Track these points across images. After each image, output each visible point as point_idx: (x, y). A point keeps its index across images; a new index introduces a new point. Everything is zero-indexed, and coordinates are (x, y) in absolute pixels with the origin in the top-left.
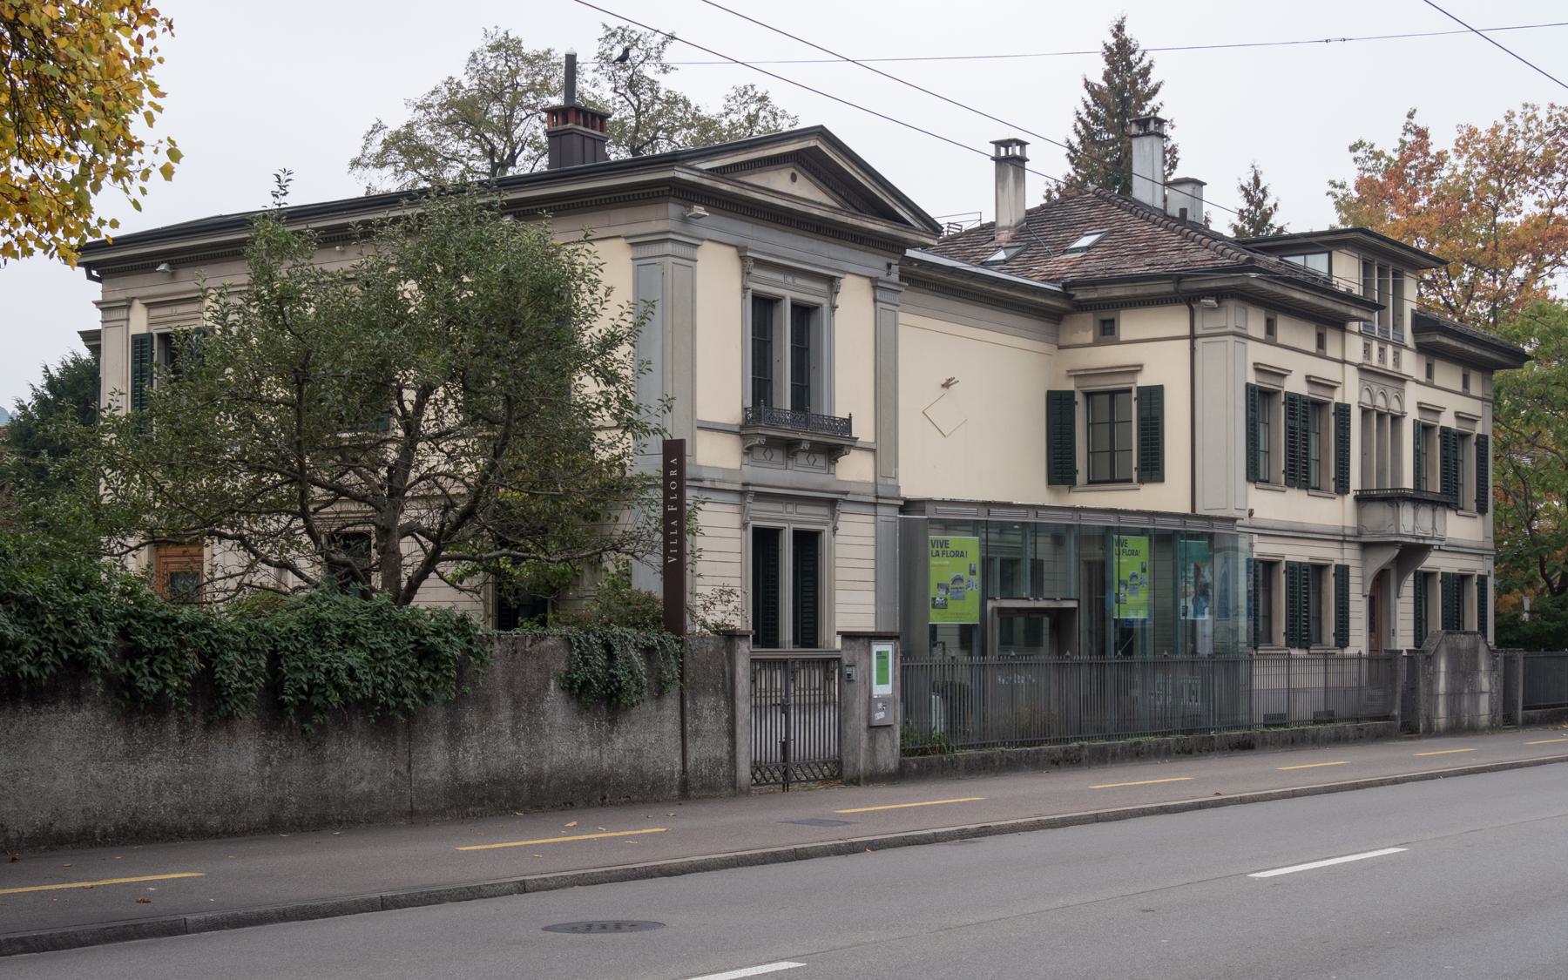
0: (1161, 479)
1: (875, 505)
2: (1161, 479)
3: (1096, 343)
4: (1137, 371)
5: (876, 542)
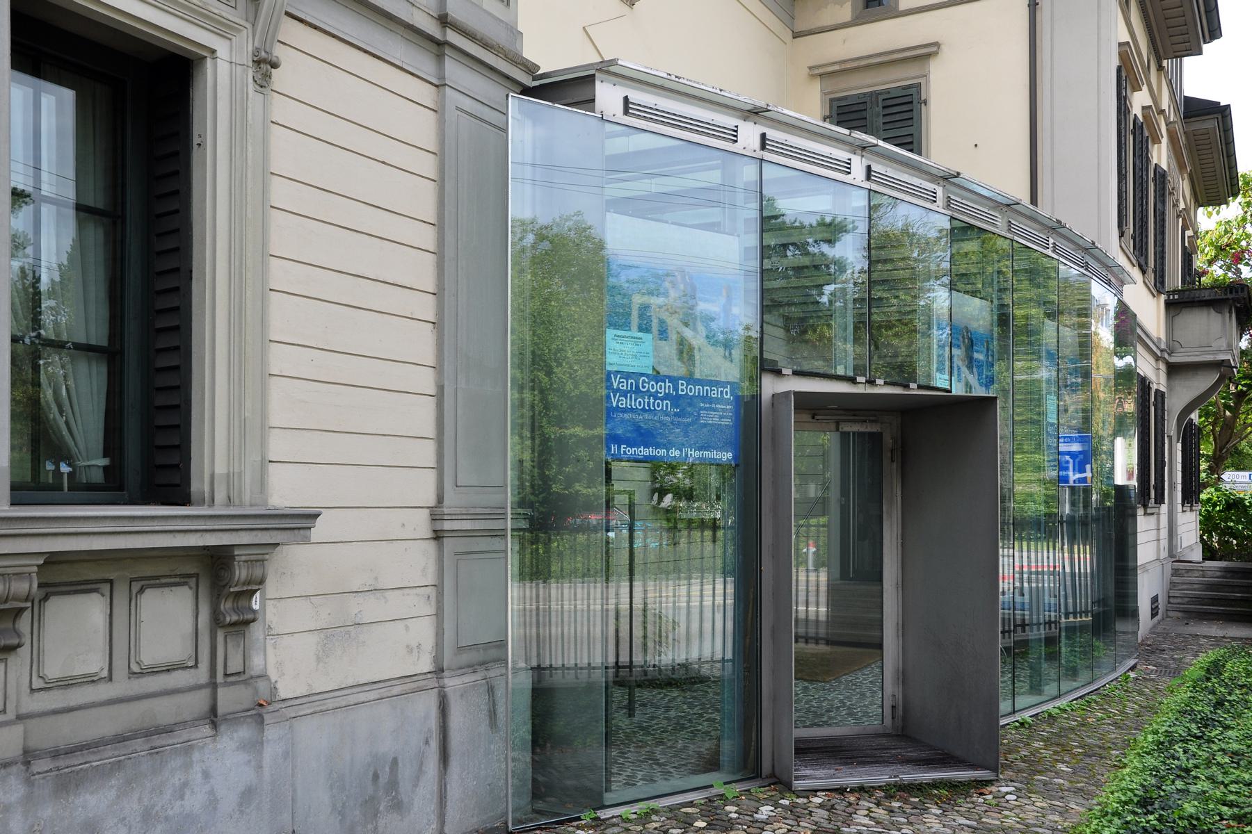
0: (1229, 105)
1: (439, 47)
2: (1229, 105)
3: (857, 21)
4: (928, 56)
5: (442, 169)
